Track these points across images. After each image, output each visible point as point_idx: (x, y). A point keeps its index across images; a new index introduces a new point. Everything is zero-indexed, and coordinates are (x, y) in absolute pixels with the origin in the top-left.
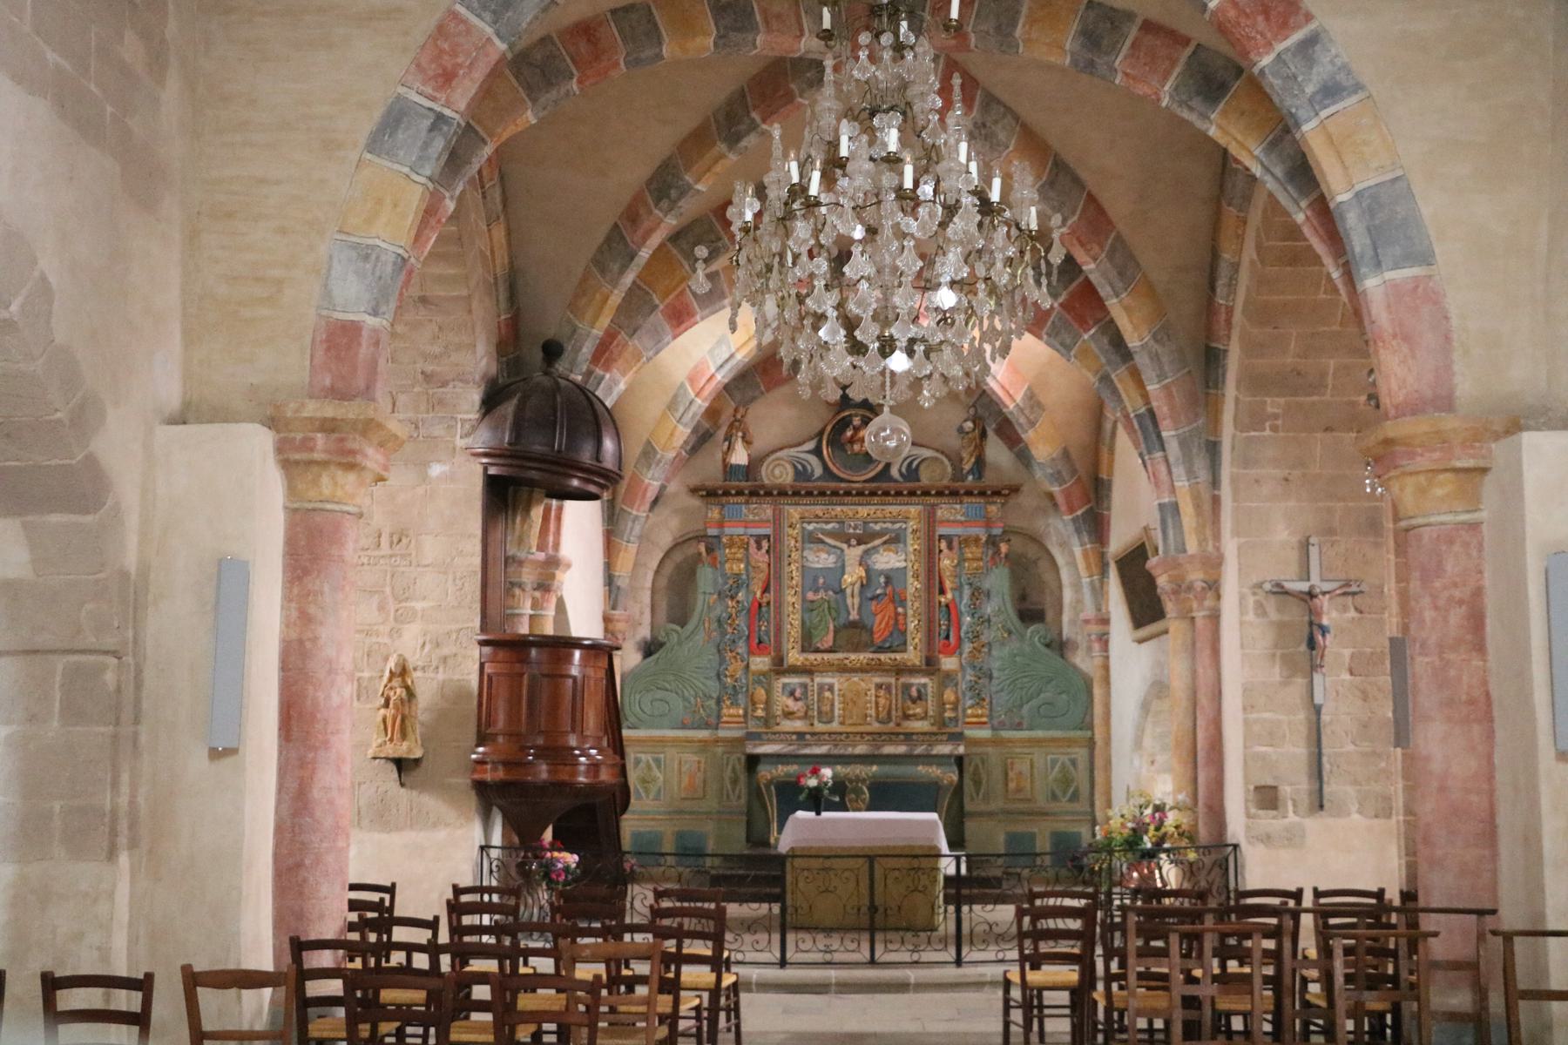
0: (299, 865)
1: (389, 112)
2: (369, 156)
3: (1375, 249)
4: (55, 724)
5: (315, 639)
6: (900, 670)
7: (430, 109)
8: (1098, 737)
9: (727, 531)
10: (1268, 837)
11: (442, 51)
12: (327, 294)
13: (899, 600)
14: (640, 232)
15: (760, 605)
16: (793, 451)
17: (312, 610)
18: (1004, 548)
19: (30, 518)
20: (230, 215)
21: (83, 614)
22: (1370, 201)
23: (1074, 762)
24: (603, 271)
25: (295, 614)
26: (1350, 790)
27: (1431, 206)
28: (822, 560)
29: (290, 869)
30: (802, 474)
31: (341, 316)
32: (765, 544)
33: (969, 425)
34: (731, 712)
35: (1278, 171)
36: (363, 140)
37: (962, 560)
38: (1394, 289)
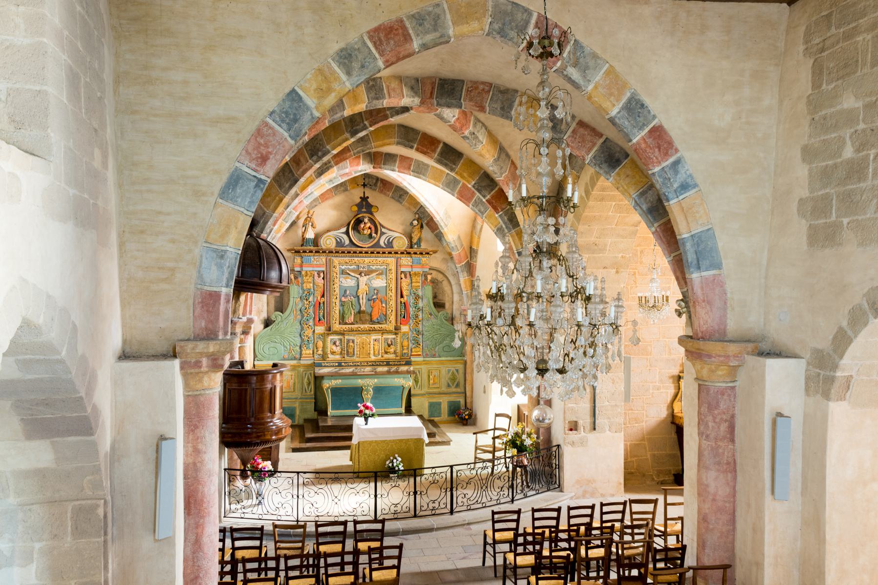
0: (197, 578)
1: (232, 176)
2: (221, 201)
3: (698, 261)
4: (69, 539)
5: (202, 462)
7: (255, 176)
9: (304, 269)
11: (259, 144)
12: (200, 277)
14: (301, 170)
16: (335, 233)
17: (200, 447)
18: (429, 277)
19: (55, 439)
20: (142, 232)
21: (85, 481)
22: (698, 239)
23: (457, 371)
24: (280, 186)
25: (191, 449)
26: (606, 421)
27: (722, 242)
28: (349, 282)
29: (192, 580)
30: (339, 243)
31: (209, 289)
32: (322, 275)
33: (415, 222)
34: (307, 352)
36: (217, 190)
38: (705, 282)
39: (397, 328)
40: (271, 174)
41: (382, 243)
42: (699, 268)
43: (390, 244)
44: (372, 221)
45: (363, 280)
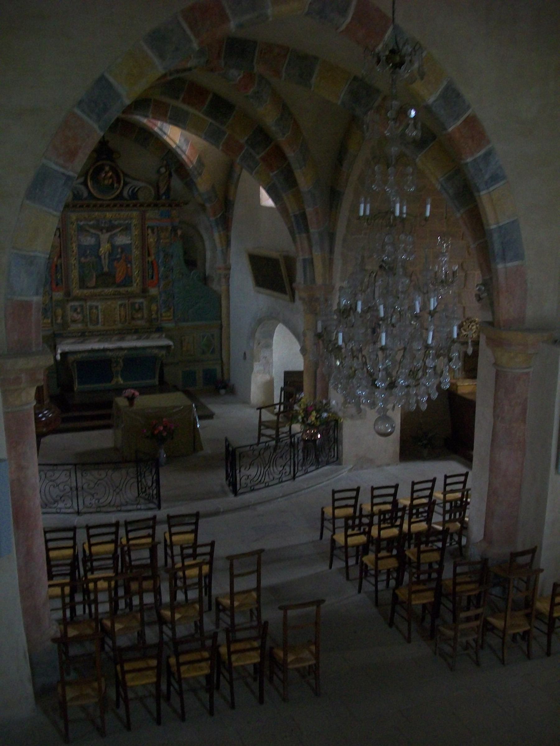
2: (28, 202)
6: (130, 296)
7: (63, 174)
8: (224, 324)
10: (352, 415)
13: (128, 261)
15: (56, 266)
18: (179, 232)
23: (213, 335)
31: (19, 298)
33: (163, 170)
35: (451, 191)
37: (159, 239)
39: (144, 291)
40: (79, 169)
41: (125, 194)
42: (504, 259)
43: (134, 195)
44: (114, 169)
45: (105, 237)
